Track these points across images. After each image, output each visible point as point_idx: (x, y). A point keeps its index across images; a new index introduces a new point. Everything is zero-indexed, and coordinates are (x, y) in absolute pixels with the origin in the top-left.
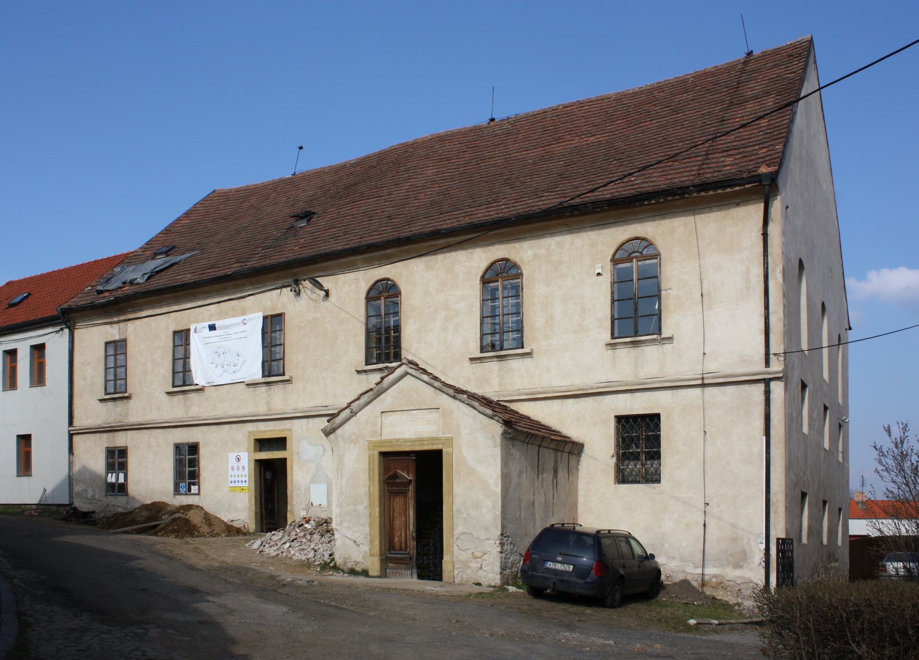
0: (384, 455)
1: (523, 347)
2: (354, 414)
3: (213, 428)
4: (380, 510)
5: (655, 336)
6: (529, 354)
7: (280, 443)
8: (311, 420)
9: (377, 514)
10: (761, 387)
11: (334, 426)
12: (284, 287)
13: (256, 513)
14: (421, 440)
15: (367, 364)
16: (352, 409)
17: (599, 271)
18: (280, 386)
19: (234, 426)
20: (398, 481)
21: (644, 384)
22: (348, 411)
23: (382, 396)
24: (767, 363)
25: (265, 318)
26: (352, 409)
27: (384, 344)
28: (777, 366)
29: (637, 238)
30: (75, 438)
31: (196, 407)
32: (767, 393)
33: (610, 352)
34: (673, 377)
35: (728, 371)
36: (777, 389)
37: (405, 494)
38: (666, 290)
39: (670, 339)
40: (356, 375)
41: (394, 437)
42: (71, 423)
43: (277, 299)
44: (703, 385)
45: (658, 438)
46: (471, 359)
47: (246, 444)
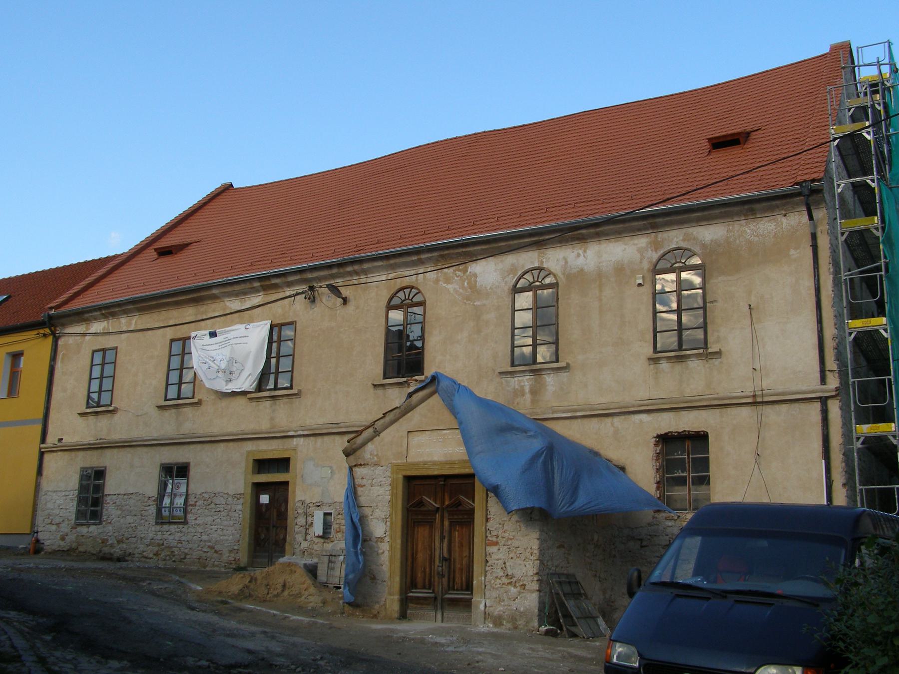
0: (409, 480)
1: (557, 361)
2: (377, 433)
3: (207, 447)
4: (402, 541)
5: (701, 351)
6: (567, 368)
7: (283, 464)
8: (319, 440)
9: (399, 546)
10: (817, 406)
11: (354, 446)
12: (298, 294)
13: (249, 544)
14: (451, 463)
15: (385, 377)
16: (375, 429)
17: (641, 281)
18: (285, 400)
19: (231, 444)
20: (423, 509)
21: (691, 401)
22: (371, 430)
23: (409, 414)
24: (823, 380)
25: (272, 327)
26: (375, 429)
27: (404, 357)
28: (833, 382)
29: (679, 249)
30: (47, 457)
31: (194, 422)
32: (825, 413)
33: (652, 366)
34: (721, 395)
35: (780, 389)
36: (835, 409)
37: (431, 524)
38: (711, 302)
39: (719, 354)
40: (372, 390)
41: (421, 460)
42: (43, 440)
43: (293, 307)
44: (755, 403)
45: (706, 461)
46: (500, 373)
47: (243, 465)
